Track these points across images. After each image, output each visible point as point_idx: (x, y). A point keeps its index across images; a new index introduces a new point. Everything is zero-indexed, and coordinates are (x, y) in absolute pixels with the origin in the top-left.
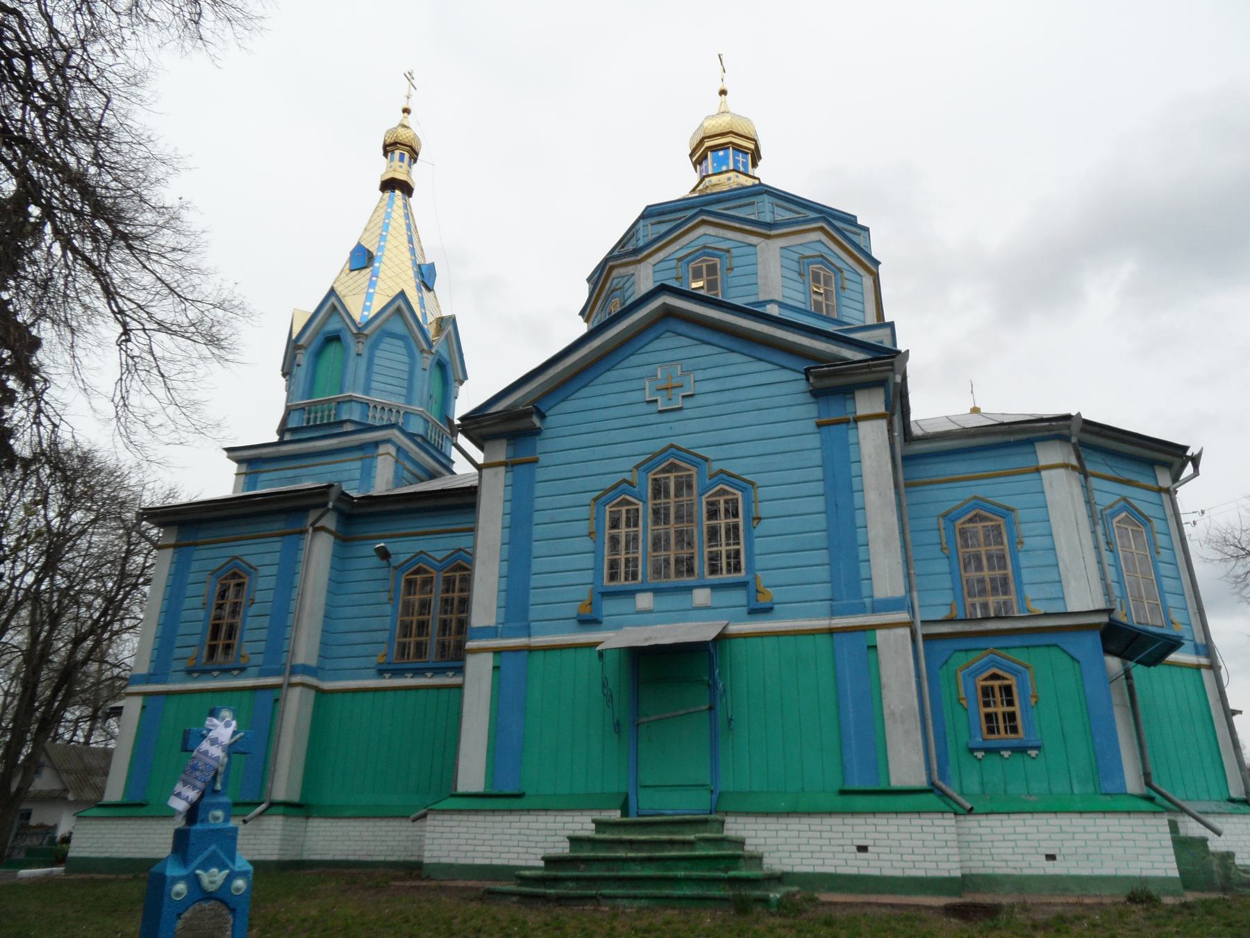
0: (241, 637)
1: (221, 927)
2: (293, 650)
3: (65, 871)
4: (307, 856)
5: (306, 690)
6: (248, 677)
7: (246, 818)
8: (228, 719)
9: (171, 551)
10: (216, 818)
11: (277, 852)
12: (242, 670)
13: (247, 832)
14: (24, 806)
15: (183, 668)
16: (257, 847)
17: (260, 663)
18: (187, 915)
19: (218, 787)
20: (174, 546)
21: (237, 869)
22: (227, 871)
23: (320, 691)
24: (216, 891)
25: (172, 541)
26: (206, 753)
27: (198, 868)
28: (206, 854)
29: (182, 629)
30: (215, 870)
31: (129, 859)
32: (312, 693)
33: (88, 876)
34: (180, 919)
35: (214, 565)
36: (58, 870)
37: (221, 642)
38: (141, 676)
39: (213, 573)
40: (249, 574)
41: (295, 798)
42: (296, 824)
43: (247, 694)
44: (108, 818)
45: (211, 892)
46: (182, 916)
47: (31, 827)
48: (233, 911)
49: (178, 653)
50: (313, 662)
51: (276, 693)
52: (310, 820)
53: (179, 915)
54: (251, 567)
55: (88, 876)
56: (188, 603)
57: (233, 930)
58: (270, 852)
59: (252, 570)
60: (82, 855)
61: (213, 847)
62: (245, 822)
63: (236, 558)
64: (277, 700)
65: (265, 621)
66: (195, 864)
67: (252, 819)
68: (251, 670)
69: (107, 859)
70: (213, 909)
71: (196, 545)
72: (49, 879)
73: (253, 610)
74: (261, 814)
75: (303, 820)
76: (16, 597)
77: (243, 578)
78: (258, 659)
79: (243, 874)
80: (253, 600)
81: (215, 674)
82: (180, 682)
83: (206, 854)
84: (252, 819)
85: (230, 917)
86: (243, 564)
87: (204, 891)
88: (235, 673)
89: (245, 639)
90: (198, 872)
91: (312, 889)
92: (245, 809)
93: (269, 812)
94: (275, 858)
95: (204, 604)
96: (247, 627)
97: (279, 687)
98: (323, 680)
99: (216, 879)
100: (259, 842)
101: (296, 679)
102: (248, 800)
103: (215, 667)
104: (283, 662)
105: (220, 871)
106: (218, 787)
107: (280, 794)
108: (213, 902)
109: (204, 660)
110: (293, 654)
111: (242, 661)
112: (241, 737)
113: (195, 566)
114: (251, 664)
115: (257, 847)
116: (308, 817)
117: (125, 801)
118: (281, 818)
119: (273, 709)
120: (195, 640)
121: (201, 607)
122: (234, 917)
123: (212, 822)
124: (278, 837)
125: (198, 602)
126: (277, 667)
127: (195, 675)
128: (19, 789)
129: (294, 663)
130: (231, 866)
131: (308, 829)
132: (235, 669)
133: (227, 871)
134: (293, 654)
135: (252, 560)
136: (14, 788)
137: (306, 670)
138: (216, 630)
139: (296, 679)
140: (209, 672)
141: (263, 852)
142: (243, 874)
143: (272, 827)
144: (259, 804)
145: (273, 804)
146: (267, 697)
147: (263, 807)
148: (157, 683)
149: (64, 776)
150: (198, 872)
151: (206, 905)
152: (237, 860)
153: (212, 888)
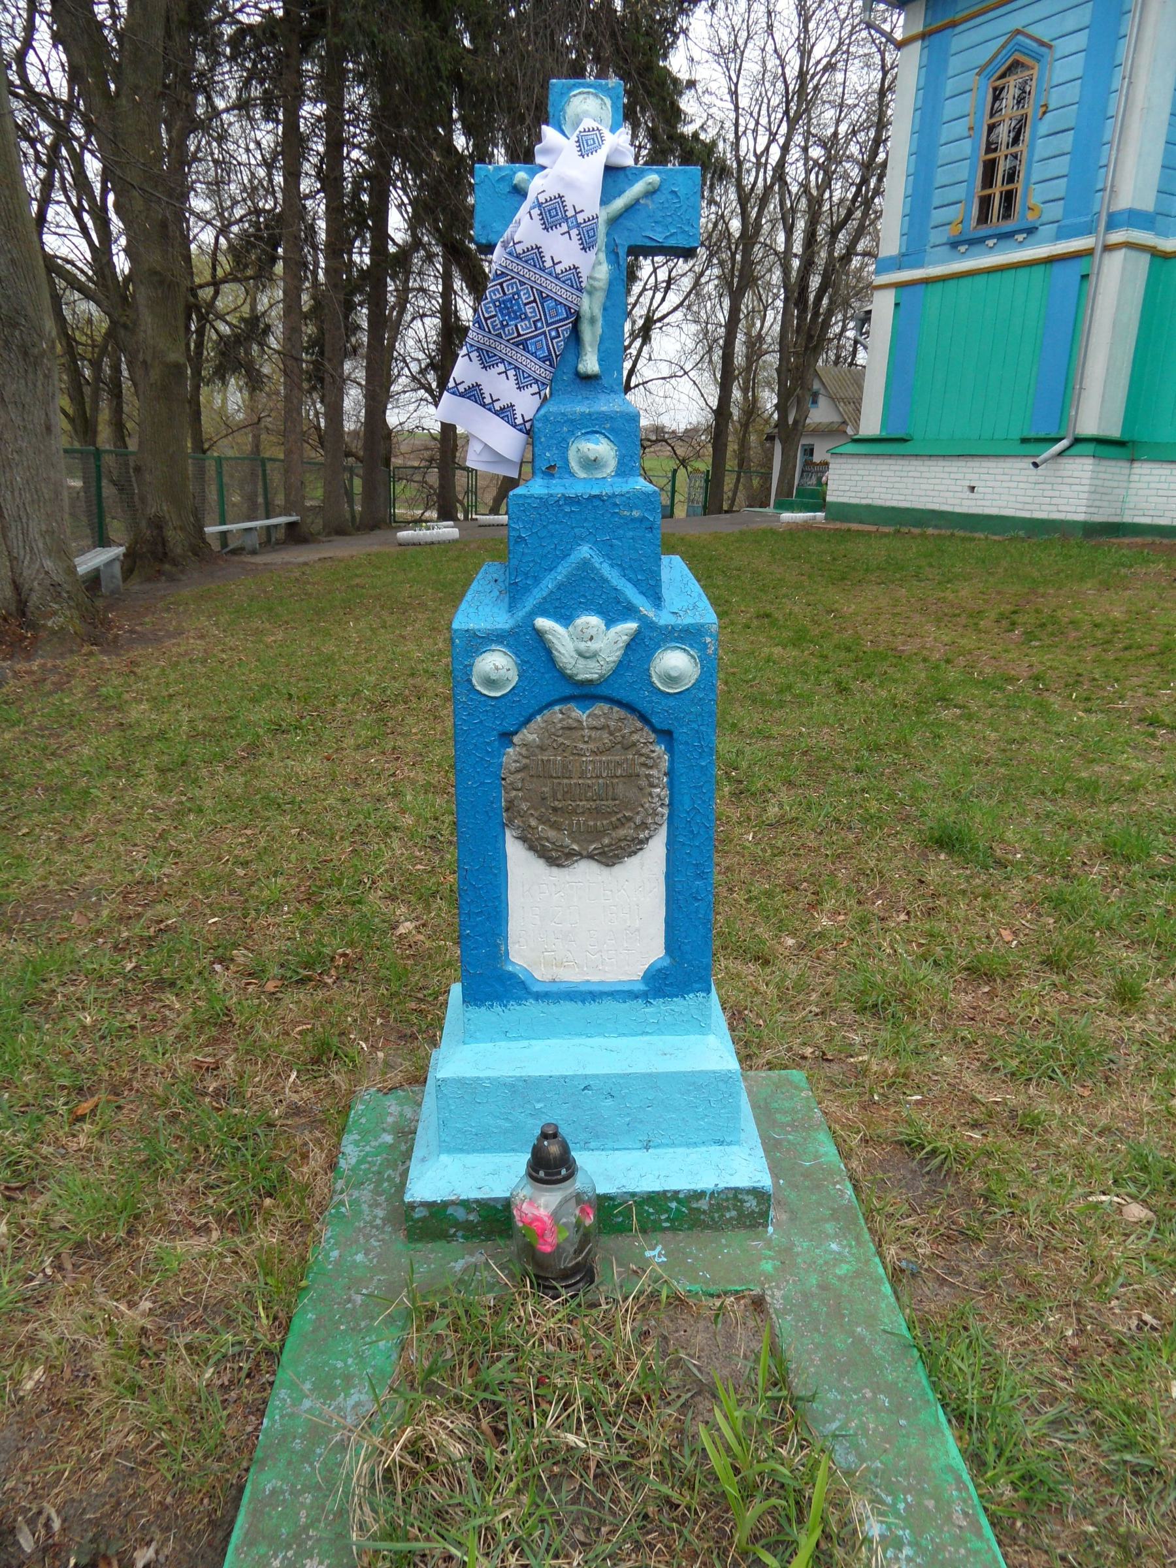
0: (1028, 174)
1: (632, 777)
2: (1112, 186)
3: (826, 518)
4: (1127, 519)
5: (1134, 254)
6: (1039, 243)
7: (1038, 460)
8: (588, 123)
9: (918, 45)
10: (592, 464)
11: (1084, 509)
12: (1031, 231)
13: (1041, 479)
14: (804, 441)
15: (944, 240)
16: (1054, 501)
17: (1059, 217)
18: (529, 735)
19: (590, 363)
20: (923, 36)
21: (664, 619)
22: (632, 626)
23: (1157, 255)
24: (604, 680)
25: (919, 28)
26: (534, 257)
27: (545, 613)
28: (562, 572)
29: (941, 177)
30: (592, 621)
31: (893, 509)
32: (1146, 258)
33: (845, 526)
34: (512, 744)
35: (983, 55)
36: (820, 515)
37: (997, 190)
38: (891, 258)
39: (982, 70)
40: (1038, 58)
41: (1114, 431)
42: (1115, 470)
43: (1039, 271)
44: (878, 456)
45: (590, 682)
46: (516, 739)
47: (815, 464)
48: (666, 735)
49: (938, 216)
50: (1147, 203)
51: (1082, 266)
52: (1136, 465)
53: (507, 737)
54: (1042, 44)
55: (845, 526)
56: (947, 133)
57: (671, 785)
58: (1073, 509)
59: (1044, 50)
60: (841, 500)
61: (584, 551)
62: (1036, 465)
63: (1018, 32)
64: (1085, 277)
65: (1066, 141)
66: (530, 602)
67: (1045, 461)
68: (1046, 231)
69: (868, 506)
70: (605, 727)
71: (953, 25)
72: (806, 528)
73: (1043, 128)
74: (1060, 454)
75: (1127, 465)
76: (765, 179)
77: (1028, 68)
78: (1055, 211)
79: (686, 636)
80: (1046, 105)
81: (991, 243)
82: (943, 262)
83: (562, 572)
84: (1045, 461)
85: (660, 749)
86: (1028, 41)
87: (569, 679)
88: (1020, 237)
89: (1034, 178)
90: (542, 623)
91: (1123, 571)
92: (1040, 446)
93: (1074, 451)
94: (1081, 517)
95: (971, 129)
96: (1036, 158)
97: (1089, 253)
98: (1165, 234)
99: (594, 646)
100: (1057, 494)
101: (1116, 237)
102: (1042, 435)
103: (990, 232)
104: (1096, 209)
105: (610, 623)
106: (590, 363)
107: (1089, 426)
108: (601, 708)
109: (974, 223)
110: (1112, 191)
111: (1030, 216)
112: (651, 193)
113: (955, 64)
114: (1044, 219)
115: (1054, 501)
116: (1133, 461)
117: (884, 435)
118: (1090, 461)
119: (1080, 290)
120: (959, 192)
121: (966, 134)
122: (670, 750)
123: (582, 474)
124: (1086, 488)
125: (960, 128)
126: (1083, 219)
127: (962, 249)
128: (796, 422)
129: (1113, 209)
130: (645, 607)
131: (1135, 478)
132: (1020, 231)
133: (632, 626)
134: (1112, 191)
135: (1042, 31)
136: (791, 422)
137: (1135, 218)
138: (990, 168)
139: (1116, 237)
140: (981, 241)
141: (1061, 508)
142: (686, 636)
143: (1076, 474)
144: (1058, 440)
145: (1077, 441)
146: (1075, 269)
147: (1064, 444)
148: (912, 267)
149: (841, 406)
150: (542, 623)
151: (578, 713)
152: (666, 593)
153: (588, 671)
